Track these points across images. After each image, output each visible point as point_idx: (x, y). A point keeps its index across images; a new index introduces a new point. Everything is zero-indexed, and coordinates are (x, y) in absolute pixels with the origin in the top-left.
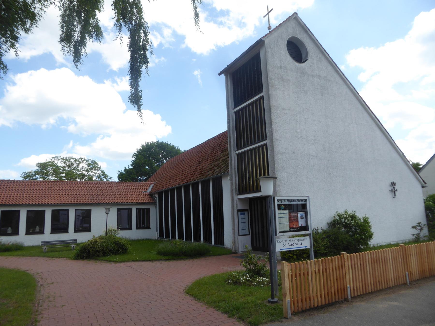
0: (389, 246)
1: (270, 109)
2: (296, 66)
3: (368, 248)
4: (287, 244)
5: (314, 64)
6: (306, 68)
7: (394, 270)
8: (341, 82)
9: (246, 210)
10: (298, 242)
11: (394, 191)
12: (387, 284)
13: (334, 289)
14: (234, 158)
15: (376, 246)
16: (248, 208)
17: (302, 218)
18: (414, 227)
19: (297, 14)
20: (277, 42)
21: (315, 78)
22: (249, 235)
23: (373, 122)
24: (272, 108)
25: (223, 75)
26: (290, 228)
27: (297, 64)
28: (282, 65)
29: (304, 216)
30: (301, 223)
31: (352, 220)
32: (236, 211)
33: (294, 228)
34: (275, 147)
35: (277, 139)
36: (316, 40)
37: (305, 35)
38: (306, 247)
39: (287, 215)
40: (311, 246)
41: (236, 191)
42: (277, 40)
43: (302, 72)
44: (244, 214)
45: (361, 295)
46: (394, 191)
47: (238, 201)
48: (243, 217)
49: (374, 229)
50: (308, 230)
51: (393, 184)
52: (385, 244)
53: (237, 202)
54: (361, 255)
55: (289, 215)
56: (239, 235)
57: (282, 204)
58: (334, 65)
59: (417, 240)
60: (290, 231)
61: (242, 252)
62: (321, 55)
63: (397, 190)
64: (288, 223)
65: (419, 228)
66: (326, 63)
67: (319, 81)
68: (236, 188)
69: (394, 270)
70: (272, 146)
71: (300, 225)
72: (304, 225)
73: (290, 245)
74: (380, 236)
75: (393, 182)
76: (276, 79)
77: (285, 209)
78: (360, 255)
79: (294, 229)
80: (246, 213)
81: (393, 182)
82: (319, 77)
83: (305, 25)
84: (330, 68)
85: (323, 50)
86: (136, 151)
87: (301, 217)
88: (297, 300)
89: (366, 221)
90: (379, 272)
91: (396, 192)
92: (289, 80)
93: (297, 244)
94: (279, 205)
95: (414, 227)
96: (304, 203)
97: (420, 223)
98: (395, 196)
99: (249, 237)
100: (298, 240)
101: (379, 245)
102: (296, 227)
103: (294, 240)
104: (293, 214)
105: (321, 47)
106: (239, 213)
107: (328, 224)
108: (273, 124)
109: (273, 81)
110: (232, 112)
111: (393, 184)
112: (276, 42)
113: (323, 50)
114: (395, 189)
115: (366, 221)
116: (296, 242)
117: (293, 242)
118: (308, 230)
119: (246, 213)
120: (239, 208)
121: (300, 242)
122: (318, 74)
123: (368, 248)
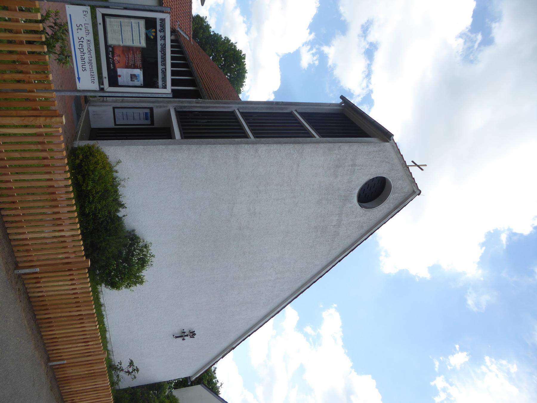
0: (103, 330)
1: (299, 143)
2: (355, 189)
3: (95, 284)
4: (82, 33)
5: (356, 217)
6: (350, 205)
7: (40, 241)
8: (330, 259)
9: (152, 123)
10: (87, 60)
11: (182, 335)
12: (12, 222)
13: (63, 349)
14: (228, 107)
15: (103, 308)
16: (156, 125)
17: (133, 77)
18: (131, 363)
19: (419, 194)
20: (386, 162)
21: (337, 218)
22: (115, 125)
23: (276, 304)
24: (301, 145)
25: (341, 101)
26: (114, 48)
27: (357, 191)
28: (357, 168)
29: (136, 83)
30: (124, 74)
31: (139, 259)
32: (151, 105)
33: (113, 56)
34: (246, 146)
35: (256, 151)
36: (385, 221)
37: (392, 206)
38: (79, 79)
39: (136, 44)
40: (80, 91)
41: (181, 107)
42: (389, 163)
43: (346, 199)
44: (147, 119)
45: (28, 293)
46: (182, 335)
47: (168, 108)
48: (142, 116)
49: (124, 292)
50: (110, 85)
51: (192, 334)
52: (106, 323)
53: (164, 107)
54: (86, 286)
55: (137, 48)
56: (114, 108)
57: (156, 32)
58: (353, 248)
59: (112, 368)
60: (107, 46)
61: (88, 112)
62: (366, 228)
63: (184, 339)
64: (121, 44)
65: (131, 370)
66: (356, 235)
67: (333, 224)
68: (185, 107)
69: (40, 241)
70: (247, 143)
71: (120, 71)
72: (120, 80)
73: (81, 39)
74: (116, 302)
75: (195, 334)
76: (339, 156)
77: (147, 38)
78: (108, 386)
79: (110, 56)
80: (149, 122)
81: (195, 334)
82: (339, 225)
83: (405, 206)
84: (349, 242)
85: (372, 231)
86: (234, 42)
87: (135, 75)
88: (42, 292)
89: (139, 281)
90: (32, 204)
91: (181, 339)
92: (336, 176)
93: (83, 59)
94: (154, 20)
95: (131, 363)
96: (160, 83)
97: (138, 370)
98: (176, 337)
99: (111, 125)
100: (90, 63)
101: (104, 313)
102: (116, 62)
103: (89, 51)
104: (138, 56)
105: (376, 228)
106: (148, 111)
107: (133, 231)
108: (279, 145)
109: (337, 152)
110: (293, 109)
111: (192, 334)
112: (387, 160)
113: (372, 231)
114: (185, 338)
115: (139, 281)
116: (86, 56)
117: (86, 51)
118: (110, 85)
119: (149, 122)
120: (155, 111)
121: (87, 66)
122: (342, 222)
123: (95, 284)
